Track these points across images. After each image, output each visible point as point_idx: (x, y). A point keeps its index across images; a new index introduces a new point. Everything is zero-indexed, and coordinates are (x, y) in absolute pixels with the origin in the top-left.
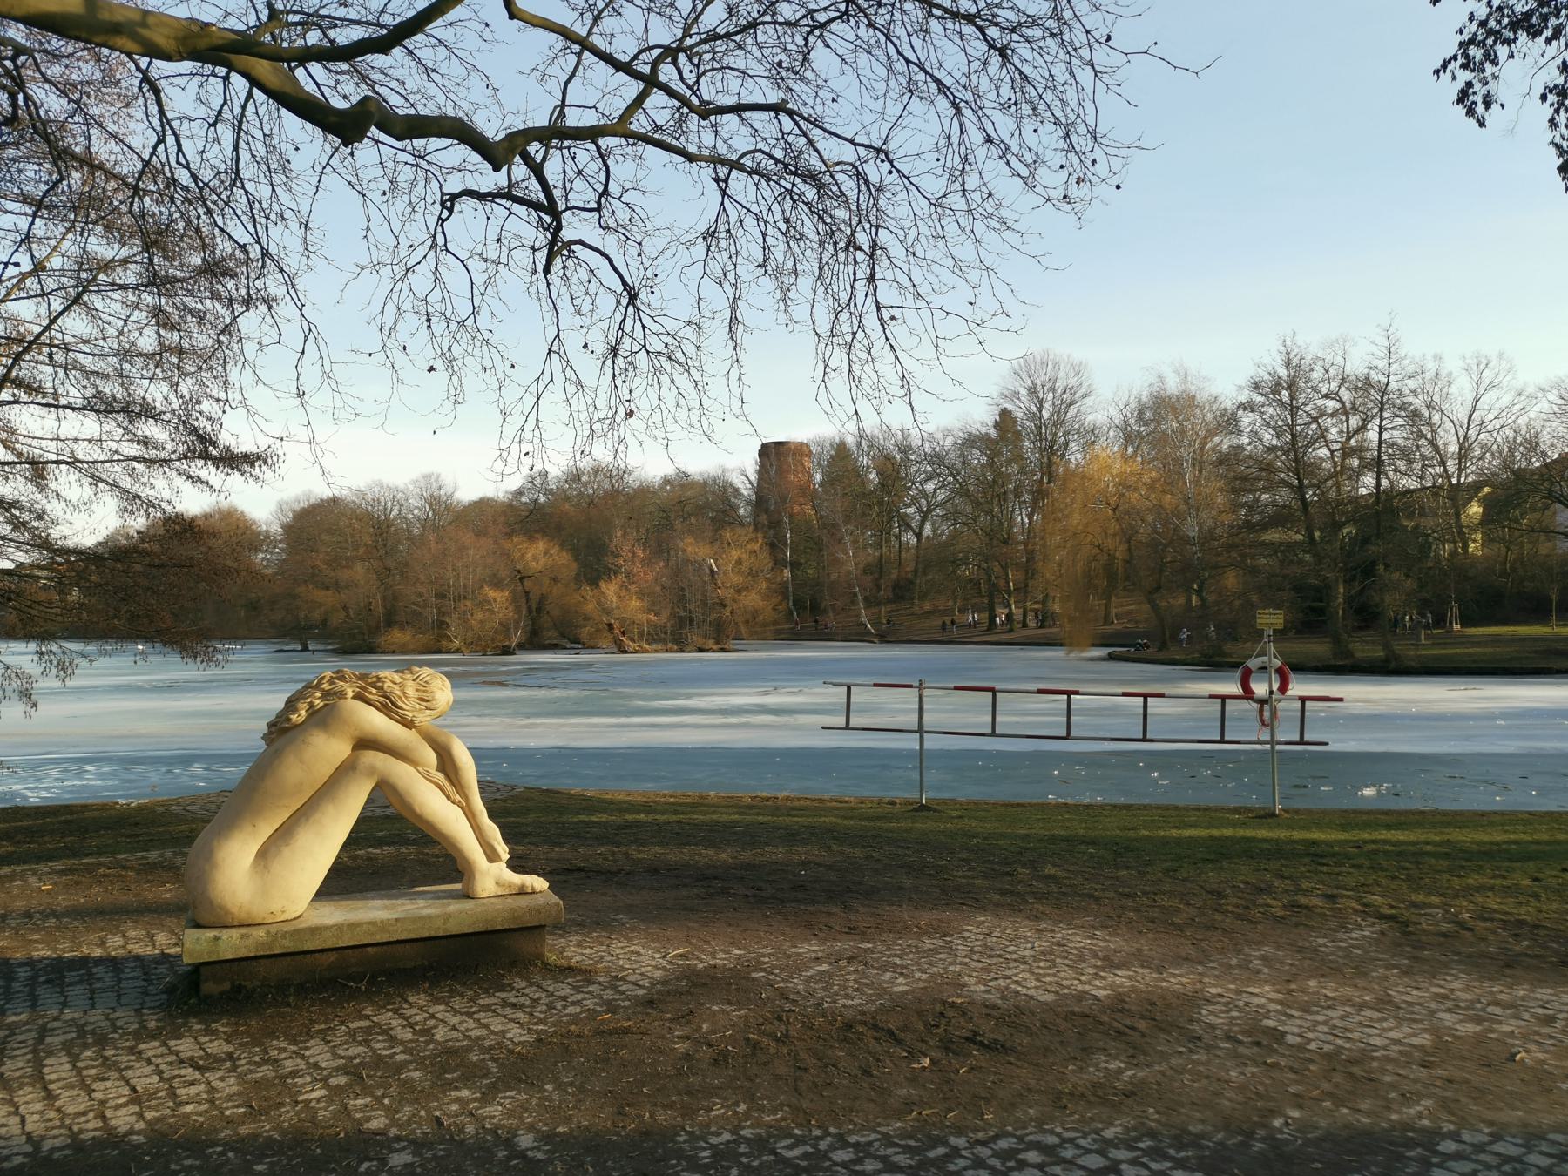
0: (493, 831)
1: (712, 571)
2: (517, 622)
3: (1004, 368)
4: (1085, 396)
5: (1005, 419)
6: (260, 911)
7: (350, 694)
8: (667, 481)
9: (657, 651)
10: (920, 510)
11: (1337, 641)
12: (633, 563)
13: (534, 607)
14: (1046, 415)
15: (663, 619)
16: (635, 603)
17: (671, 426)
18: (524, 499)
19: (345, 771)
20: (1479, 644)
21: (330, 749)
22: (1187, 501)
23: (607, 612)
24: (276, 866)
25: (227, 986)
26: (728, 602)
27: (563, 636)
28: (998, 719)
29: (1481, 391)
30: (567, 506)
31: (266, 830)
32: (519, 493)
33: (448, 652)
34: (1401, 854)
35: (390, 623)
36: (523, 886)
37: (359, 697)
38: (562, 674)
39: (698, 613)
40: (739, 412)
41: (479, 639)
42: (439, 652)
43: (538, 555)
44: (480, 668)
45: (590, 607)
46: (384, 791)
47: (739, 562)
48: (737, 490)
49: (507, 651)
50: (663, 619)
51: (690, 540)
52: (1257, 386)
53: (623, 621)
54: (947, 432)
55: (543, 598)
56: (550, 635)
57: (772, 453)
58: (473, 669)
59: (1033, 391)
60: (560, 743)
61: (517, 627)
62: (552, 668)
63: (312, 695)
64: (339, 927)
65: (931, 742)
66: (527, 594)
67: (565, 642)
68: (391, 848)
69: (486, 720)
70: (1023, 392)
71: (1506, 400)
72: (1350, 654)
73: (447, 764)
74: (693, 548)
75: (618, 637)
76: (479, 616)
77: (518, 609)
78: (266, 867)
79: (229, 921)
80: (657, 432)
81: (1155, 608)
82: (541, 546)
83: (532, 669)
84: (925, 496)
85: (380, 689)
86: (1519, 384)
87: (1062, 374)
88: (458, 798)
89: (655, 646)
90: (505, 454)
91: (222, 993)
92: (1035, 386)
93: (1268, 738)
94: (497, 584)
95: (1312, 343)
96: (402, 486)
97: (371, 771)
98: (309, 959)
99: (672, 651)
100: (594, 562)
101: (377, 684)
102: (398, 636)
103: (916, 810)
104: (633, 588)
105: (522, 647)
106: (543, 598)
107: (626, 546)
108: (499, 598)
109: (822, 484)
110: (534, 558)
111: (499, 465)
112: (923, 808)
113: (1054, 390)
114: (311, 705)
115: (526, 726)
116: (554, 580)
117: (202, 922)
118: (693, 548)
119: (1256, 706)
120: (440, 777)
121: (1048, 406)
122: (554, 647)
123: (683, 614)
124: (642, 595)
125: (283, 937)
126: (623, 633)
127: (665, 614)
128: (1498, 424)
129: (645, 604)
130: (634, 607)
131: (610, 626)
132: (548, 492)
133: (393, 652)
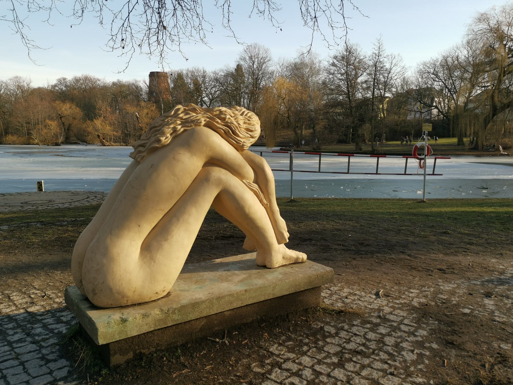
0: (282, 223)
1: (137, 117)
2: (61, 134)
3: (241, 49)
4: (269, 61)
5: (239, 68)
6: (149, 294)
7: (203, 123)
8: (114, 84)
9: (117, 146)
10: (209, 98)
11: (357, 144)
12: (106, 113)
13: (66, 129)
14: (255, 66)
15: (119, 134)
16: (108, 128)
17: (181, 35)
18: (57, 88)
19: (201, 181)
20: (393, 146)
21: (191, 164)
22: (310, 97)
23: (97, 131)
24: (160, 257)
25: (131, 355)
26: (144, 128)
27: (79, 139)
28: (318, 166)
29: (392, 66)
30: (75, 91)
31: (147, 228)
32: (55, 86)
33: (33, 144)
34: (498, 216)
35: (7, 133)
36: (298, 258)
37: (208, 125)
38: (85, 153)
39: (132, 132)
40: (226, 25)
41: (46, 140)
42: (29, 144)
43: (67, 109)
44: (49, 150)
45: (90, 129)
46: (225, 197)
47: (147, 114)
48: (141, 88)
49: (57, 144)
50: (119, 134)
51: (129, 105)
52: (335, 57)
53: (104, 134)
54: (222, 70)
55: (70, 125)
56: (73, 139)
57: (153, 75)
58: (47, 150)
59: (251, 58)
60: (105, 177)
61: (61, 135)
62: (79, 151)
63: (174, 122)
64: (210, 301)
65: (297, 176)
66: (63, 123)
67: (79, 142)
68: (224, 237)
69: (65, 169)
70: (247, 58)
71: (399, 70)
72: (361, 149)
73: (260, 178)
74: (130, 109)
75: (103, 140)
76: (45, 131)
77: (61, 129)
78: (152, 259)
79: (124, 302)
80: (174, 37)
81: (296, 133)
82: (68, 105)
83: (71, 151)
84: (211, 94)
85: (223, 120)
86: (403, 65)
87: (261, 52)
88: (265, 202)
89: (116, 144)
90: (114, 38)
91: (128, 362)
92: (252, 56)
93: (423, 173)
94: (51, 119)
95: (483, 8)
96: (5, 81)
97: (219, 182)
98: (187, 326)
99: (122, 146)
100: (90, 111)
101: (220, 115)
102: (10, 138)
103: (289, 202)
104: (107, 122)
105: (63, 143)
106: (70, 125)
107: (103, 106)
108: (54, 125)
109: (173, 88)
110: (66, 110)
111: (111, 43)
112: (292, 201)
113: (258, 58)
114: (175, 130)
115: (84, 171)
116: (74, 118)
117: (100, 305)
118: (130, 109)
119: (418, 161)
120: (255, 187)
121: (256, 63)
122: (75, 143)
123: (126, 132)
124: (110, 125)
125: (174, 313)
126: (104, 139)
127: (120, 132)
128: (396, 77)
129: (112, 128)
130: (108, 129)
131: (98, 136)
132: (66, 86)
133: (10, 144)
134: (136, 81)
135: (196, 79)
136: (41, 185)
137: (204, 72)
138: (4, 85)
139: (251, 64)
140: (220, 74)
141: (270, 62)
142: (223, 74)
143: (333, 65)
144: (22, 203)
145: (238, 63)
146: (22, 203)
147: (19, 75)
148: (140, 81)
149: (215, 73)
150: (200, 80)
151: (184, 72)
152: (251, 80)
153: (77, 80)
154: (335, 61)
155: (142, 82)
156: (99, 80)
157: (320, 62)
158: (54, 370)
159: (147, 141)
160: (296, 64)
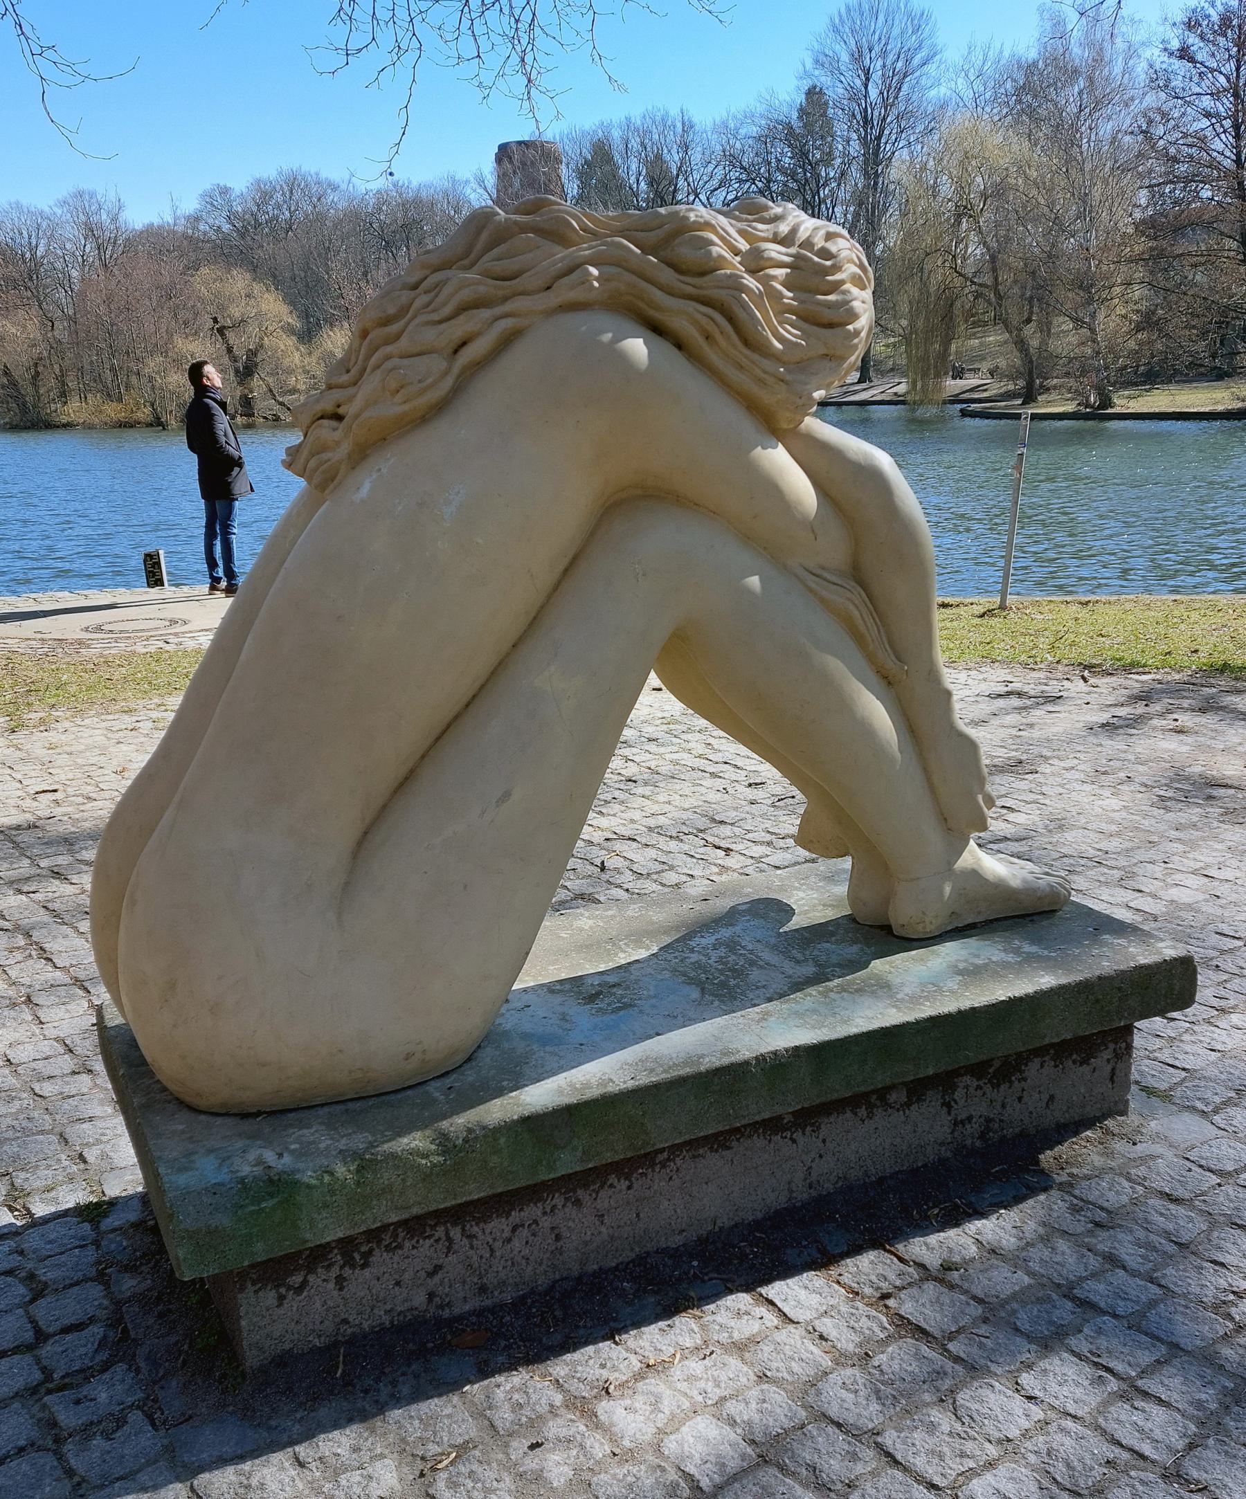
5: (814, 95)
14: (873, 93)
54: (749, 116)
59: (857, 57)
70: (845, 57)
121: (876, 77)
134: (454, 181)
135: (659, 157)
136: (159, 563)
137: (688, 127)
138: (44, 225)
139: (858, 82)
140: (743, 131)
141: (931, 68)
142: (754, 130)
143: (1185, 54)
144: (87, 629)
145: (806, 84)
146: (87, 629)
147: (86, 186)
148: (467, 182)
149: (723, 128)
150: (673, 159)
151: (616, 134)
152: (855, 148)
153: (264, 194)
154: (1193, 39)
155: (474, 185)
156: (335, 188)
157: (1131, 52)
158: (51, 1330)
159: (351, 391)
160: (1030, 68)
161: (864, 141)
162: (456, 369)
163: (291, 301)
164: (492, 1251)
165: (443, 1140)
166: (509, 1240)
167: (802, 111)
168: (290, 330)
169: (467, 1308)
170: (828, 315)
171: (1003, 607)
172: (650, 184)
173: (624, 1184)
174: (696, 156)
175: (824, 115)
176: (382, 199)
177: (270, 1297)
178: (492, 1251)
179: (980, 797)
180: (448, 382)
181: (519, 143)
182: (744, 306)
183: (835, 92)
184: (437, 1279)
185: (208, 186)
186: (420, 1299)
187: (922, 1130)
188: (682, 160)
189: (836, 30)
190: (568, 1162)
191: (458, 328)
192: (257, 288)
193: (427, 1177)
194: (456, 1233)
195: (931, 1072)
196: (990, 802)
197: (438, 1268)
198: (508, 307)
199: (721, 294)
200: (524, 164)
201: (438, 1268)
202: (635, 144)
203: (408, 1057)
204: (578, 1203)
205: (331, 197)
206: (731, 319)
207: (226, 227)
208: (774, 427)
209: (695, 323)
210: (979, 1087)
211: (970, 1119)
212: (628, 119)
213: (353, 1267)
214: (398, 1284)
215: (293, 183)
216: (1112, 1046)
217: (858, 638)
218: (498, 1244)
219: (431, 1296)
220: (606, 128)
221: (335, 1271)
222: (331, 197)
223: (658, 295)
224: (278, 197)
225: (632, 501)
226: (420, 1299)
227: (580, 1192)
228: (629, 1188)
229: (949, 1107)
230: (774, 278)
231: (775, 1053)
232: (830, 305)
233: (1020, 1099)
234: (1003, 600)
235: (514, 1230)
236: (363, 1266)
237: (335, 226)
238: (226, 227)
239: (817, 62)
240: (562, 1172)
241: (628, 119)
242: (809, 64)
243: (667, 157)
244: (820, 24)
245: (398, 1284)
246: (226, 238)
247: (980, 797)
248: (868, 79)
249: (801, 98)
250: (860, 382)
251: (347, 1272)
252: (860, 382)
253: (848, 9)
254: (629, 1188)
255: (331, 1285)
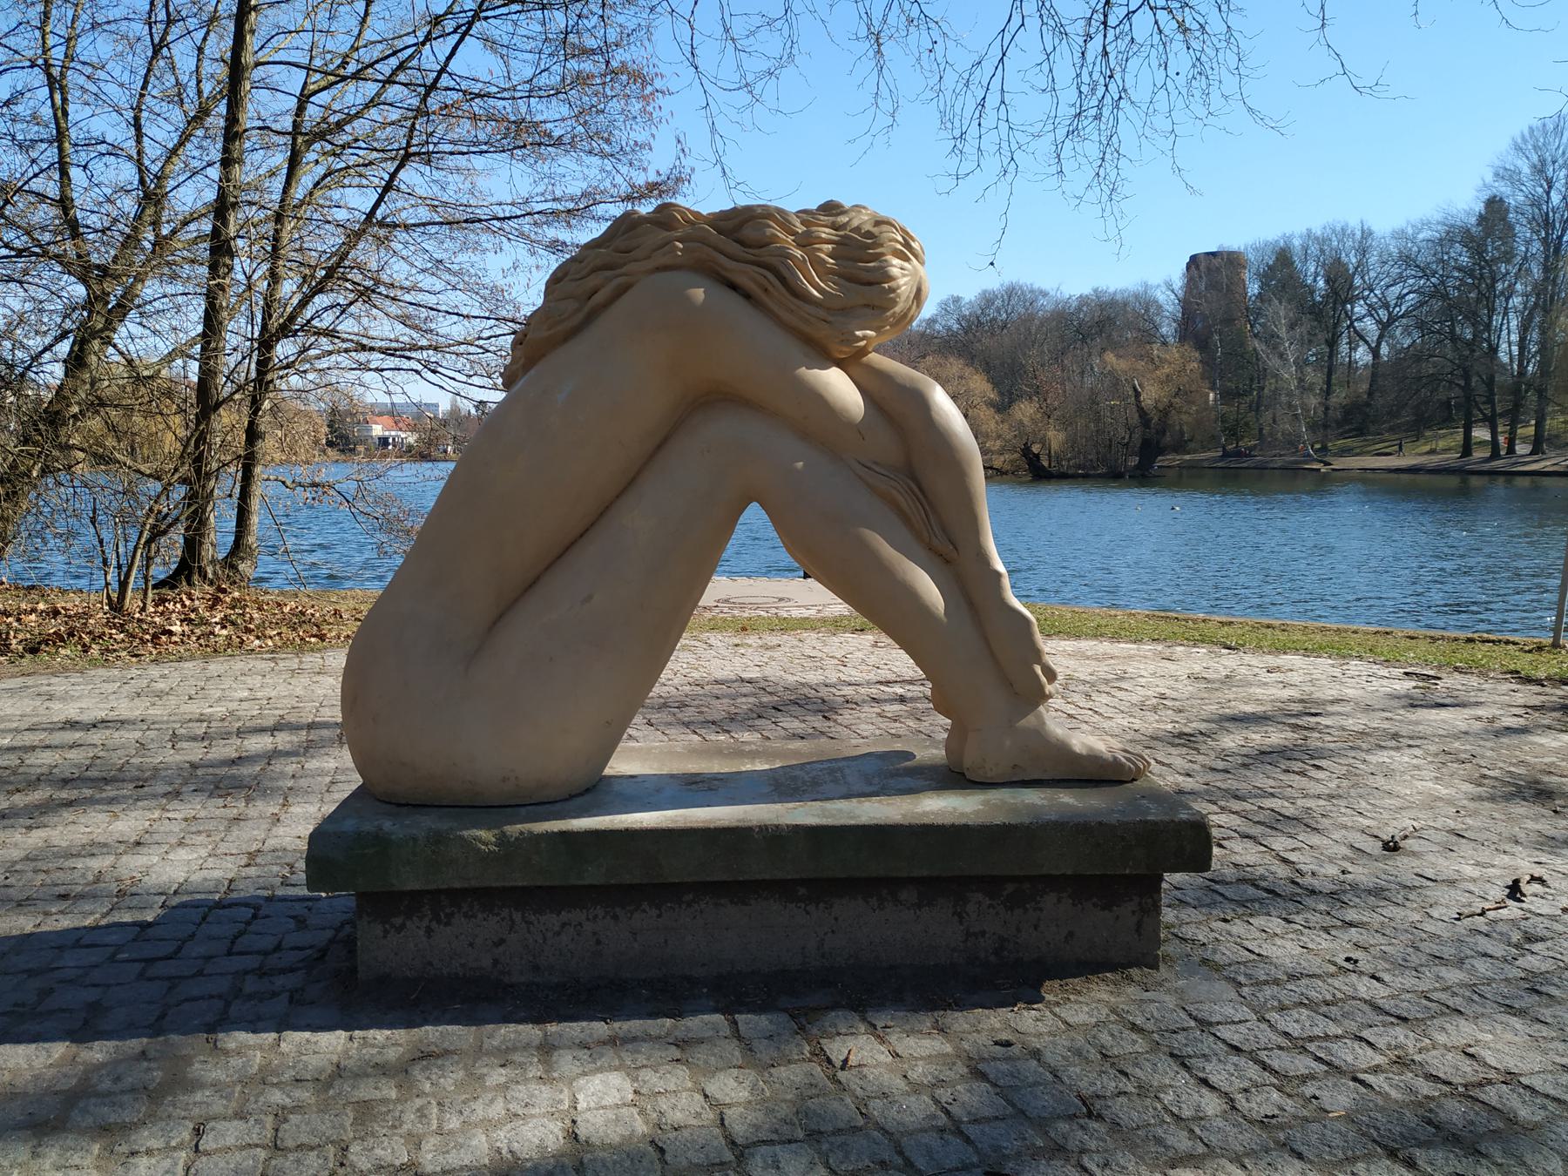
5: (1495, 206)
54: (1426, 224)
59: (1539, 169)
70: (1526, 170)
137: (1367, 234)
140: (1421, 236)
145: (1486, 195)
149: (1399, 235)
151: (1297, 242)
152: (1536, 247)
153: (988, 300)
156: (1045, 294)
161: (1545, 241)
162: (586, 309)
163: (995, 383)
164: (545, 939)
165: (502, 840)
166: (558, 934)
167: (1482, 219)
168: (991, 404)
169: (523, 979)
170: (865, 276)
171: (1556, 645)
172: (1327, 282)
173: (654, 912)
174: (1373, 259)
175: (1504, 219)
176: (1083, 301)
177: (378, 929)
178: (545, 939)
179: (1038, 669)
180: (581, 316)
181: (1208, 254)
182: (788, 267)
183: (1515, 198)
184: (501, 949)
185: (945, 297)
186: (486, 962)
187: (932, 929)
188: (1360, 263)
189: (1518, 148)
190: (593, 875)
191: (593, 281)
192: (968, 371)
193: (486, 858)
194: (517, 916)
195: (925, 873)
196: (1051, 675)
197: (502, 941)
198: (624, 270)
199: (773, 261)
200: (1209, 269)
201: (502, 941)
202: (1314, 249)
203: (504, 780)
204: (615, 917)
205: (1042, 301)
206: (783, 280)
207: (955, 327)
208: (828, 359)
209: (755, 282)
210: (990, 906)
211: (983, 933)
212: (1309, 231)
213: (439, 922)
214: (471, 945)
215: (1011, 292)
216: (1136, 899)
217: (906, 520)
218: (549, 934)
219: (496, 962)
220: (1288, 239)
221: (425, 922)
222: (1042, 301)
223: (722, 259)
224: (998, 303)
225: (710, 399)
226: (486, 962)
227: (618, 910)
228: (659, 916)
229: (960, 916)
230: (820, 250)
231: (777, 826)
232: (868, 270)
233: (1036, 927)
234: (1556, 637)
235: (564, 925)
236: (447, 924)
237: (1042, 324)
238: (955, 327)
239: (1496, 175)
240: (586, 882)
241: (1309, 231)
242: (1489, 178)
243: (1344, 258)
244: (1504, 144)
245: (471, 945)
246: (955, 334)
247: (1038, 669)
248: (1550, 187)
249: (1479, 207)
250: (1531, 454)
251: (434, 925)
252: (1531, 454)
253: (1531, 129)
254: (659, 916)
255: (421, 933)
